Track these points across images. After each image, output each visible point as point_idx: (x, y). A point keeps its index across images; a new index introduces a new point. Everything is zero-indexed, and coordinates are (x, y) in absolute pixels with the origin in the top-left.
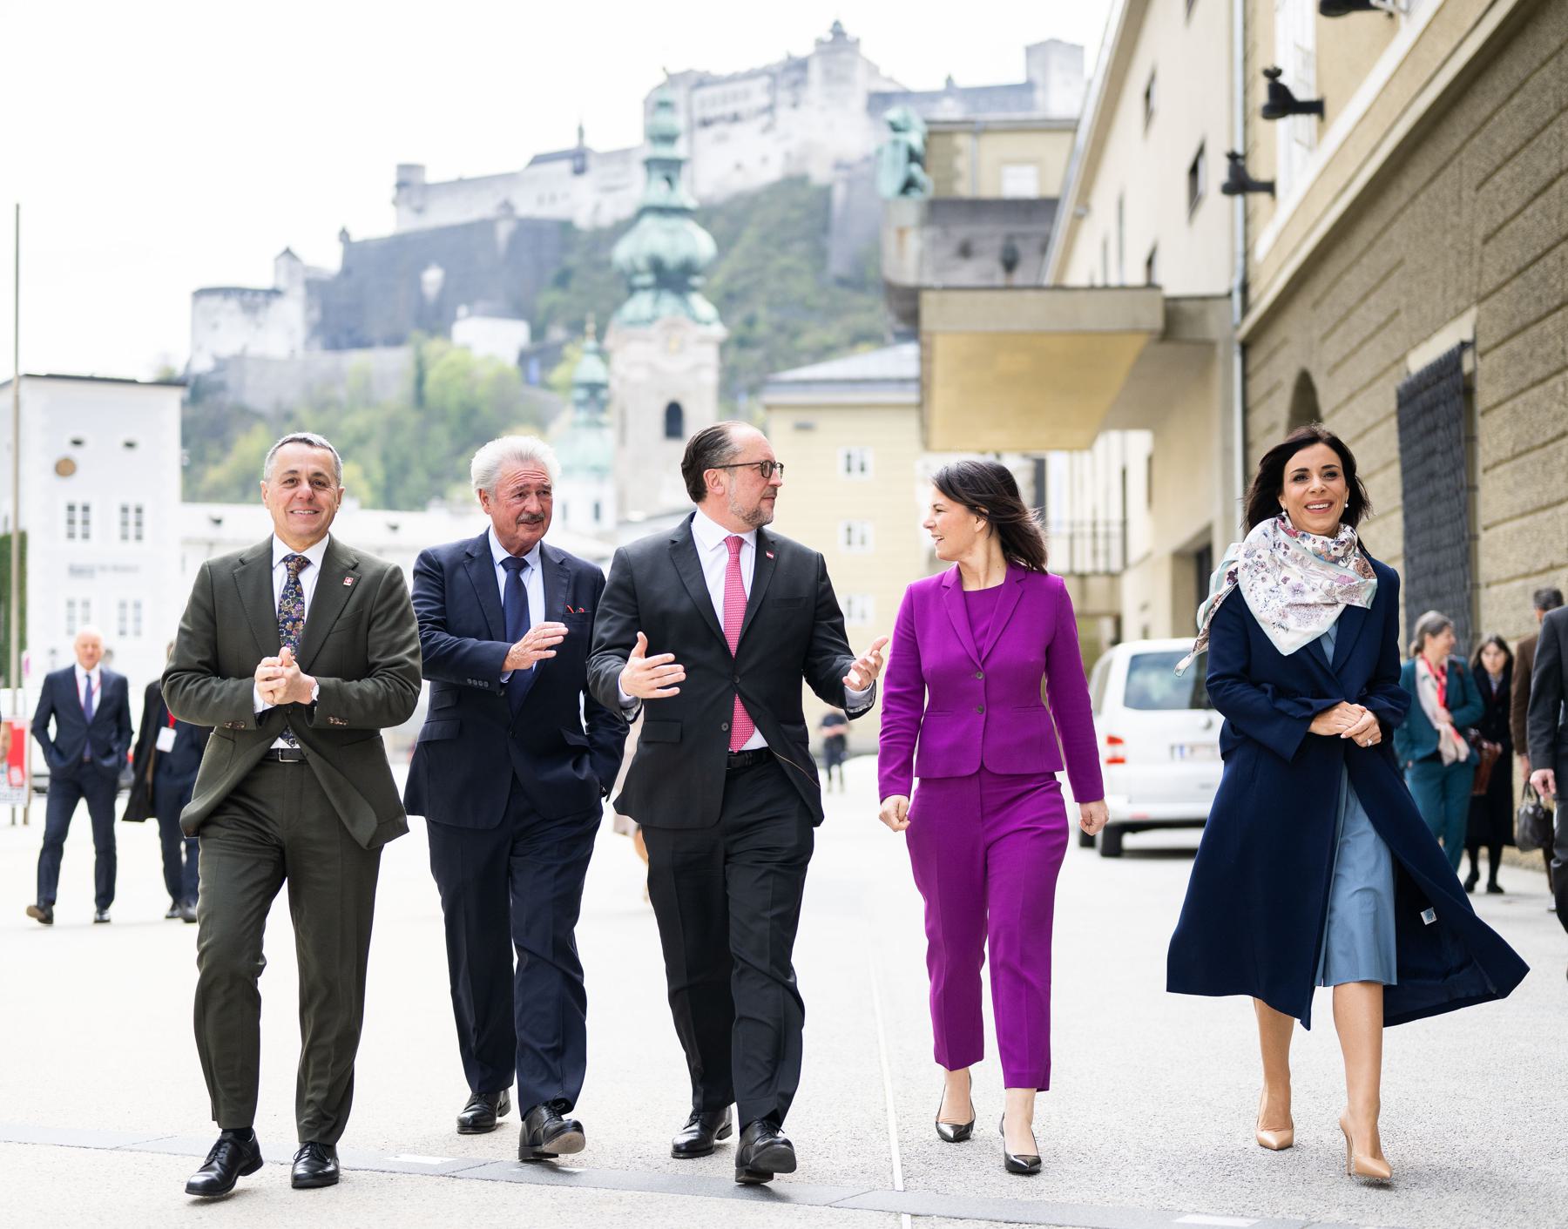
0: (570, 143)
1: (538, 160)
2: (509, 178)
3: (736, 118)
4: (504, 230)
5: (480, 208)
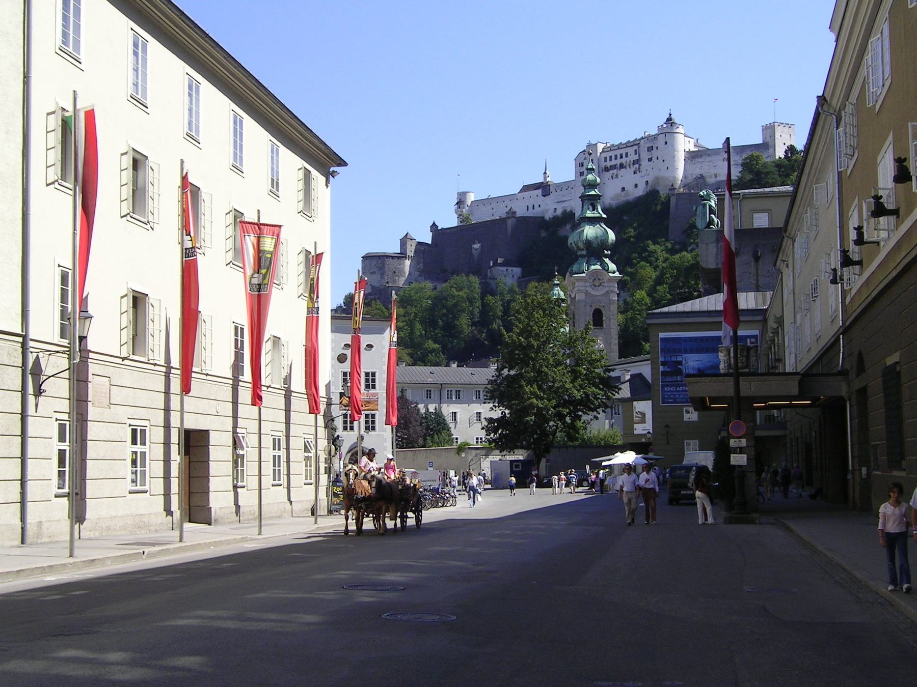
0: (540, 179)
1: (526, 188)
2: (511, 197)
3: (622, 166)
4: (510, 222)
5: (500, 212)
